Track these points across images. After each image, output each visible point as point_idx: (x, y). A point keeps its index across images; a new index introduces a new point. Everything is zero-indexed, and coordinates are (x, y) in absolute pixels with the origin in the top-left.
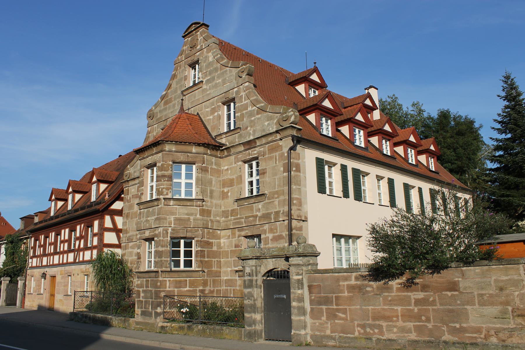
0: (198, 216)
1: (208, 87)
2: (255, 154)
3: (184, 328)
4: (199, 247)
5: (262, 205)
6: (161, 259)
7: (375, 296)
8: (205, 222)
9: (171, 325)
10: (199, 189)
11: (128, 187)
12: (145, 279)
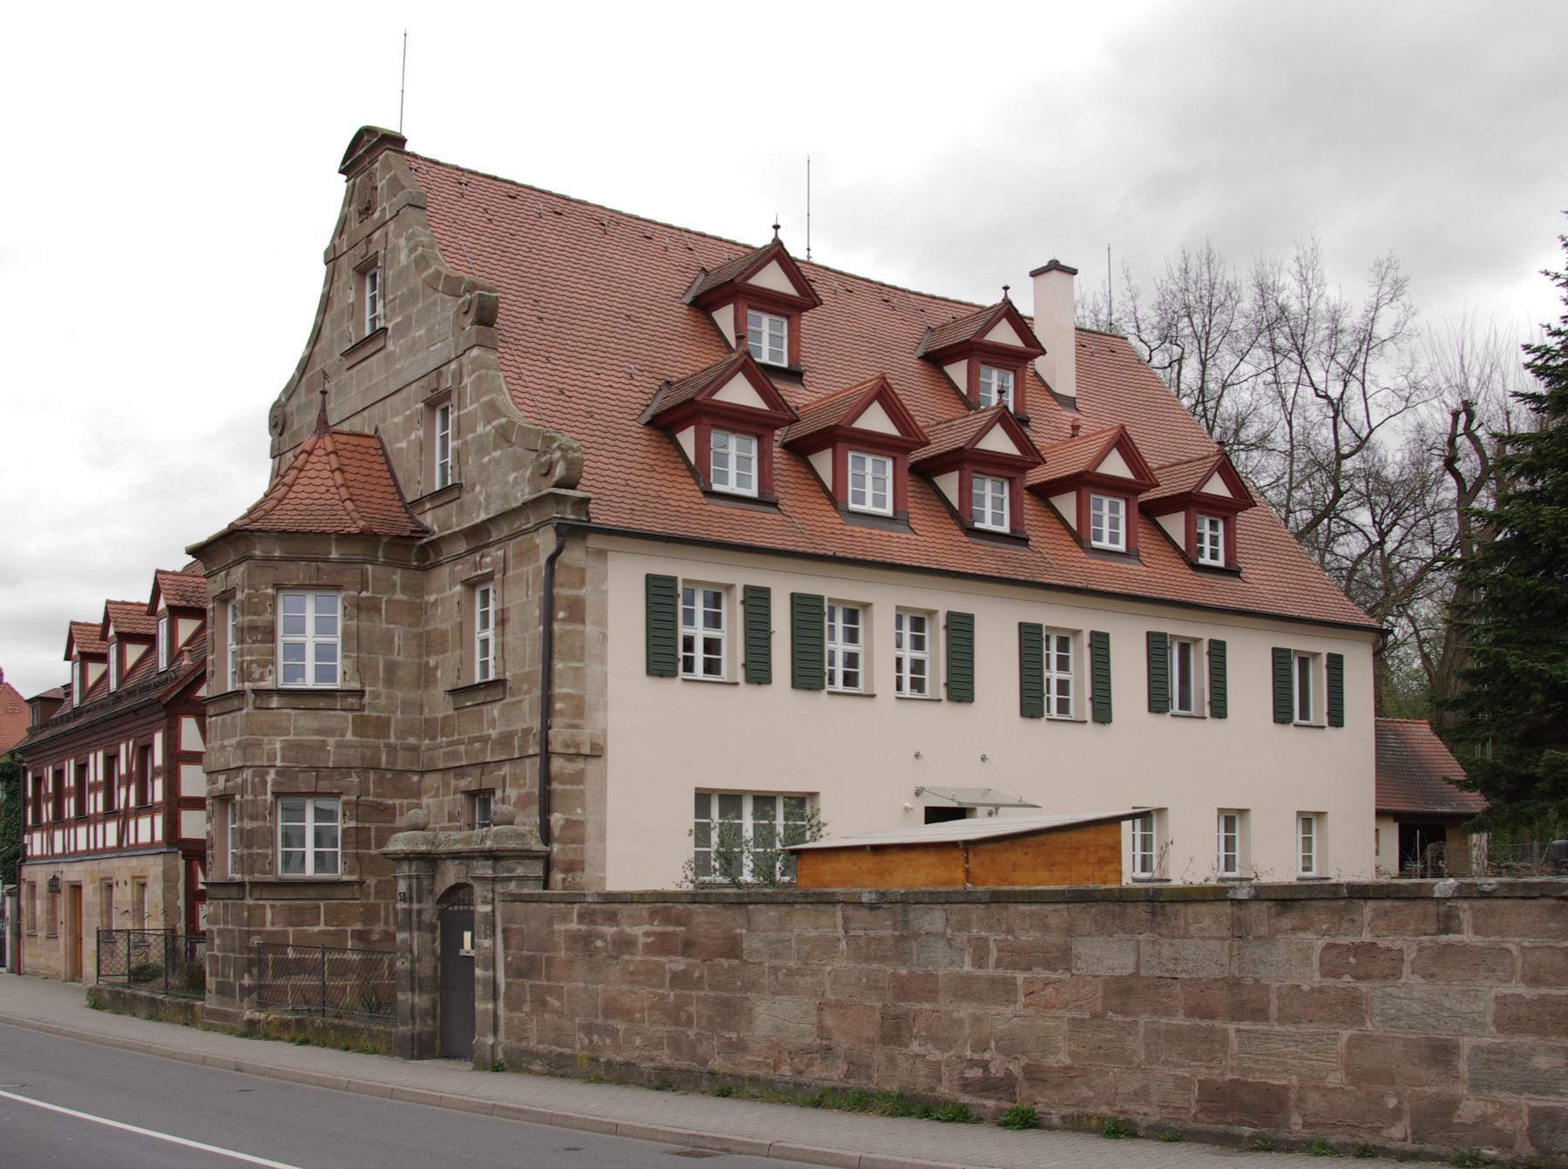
0: (349, 736)
1: (398, 350)
4: (351, 820)
6: (250, 851)
7: (609, 961)
8: (368, 753)
10: (349, 662)
12: (221, 902)
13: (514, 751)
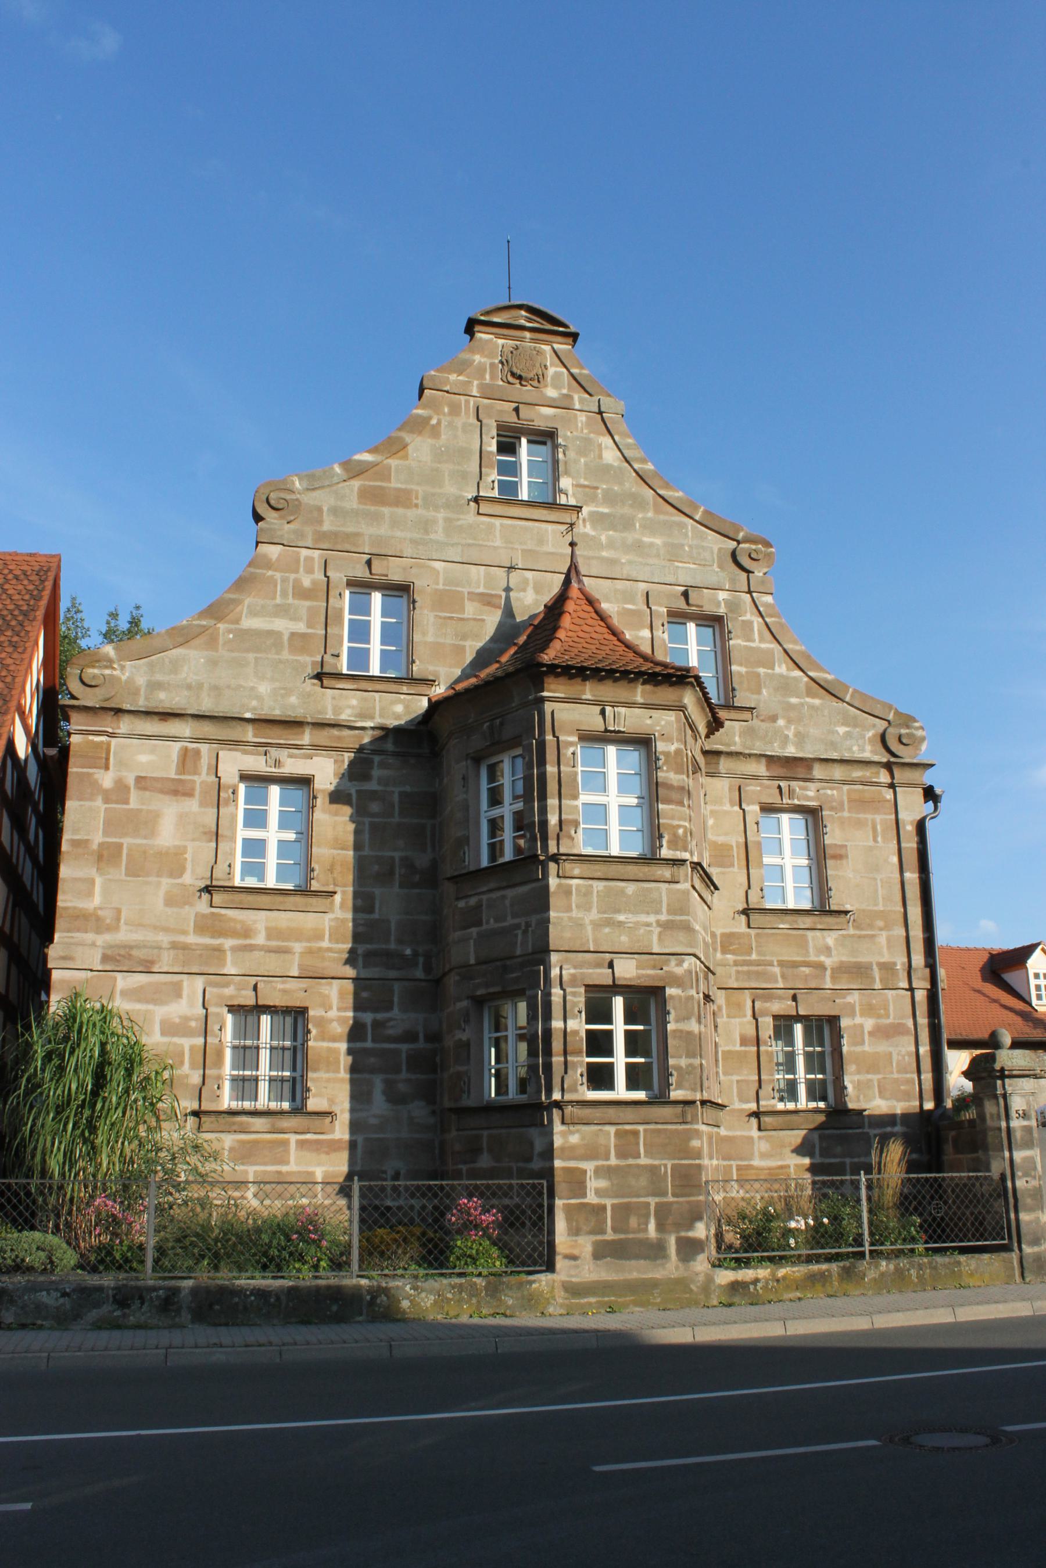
2: (808, 798)
5: (836, 939)
9: (773, 1274)
11: (112, 735)
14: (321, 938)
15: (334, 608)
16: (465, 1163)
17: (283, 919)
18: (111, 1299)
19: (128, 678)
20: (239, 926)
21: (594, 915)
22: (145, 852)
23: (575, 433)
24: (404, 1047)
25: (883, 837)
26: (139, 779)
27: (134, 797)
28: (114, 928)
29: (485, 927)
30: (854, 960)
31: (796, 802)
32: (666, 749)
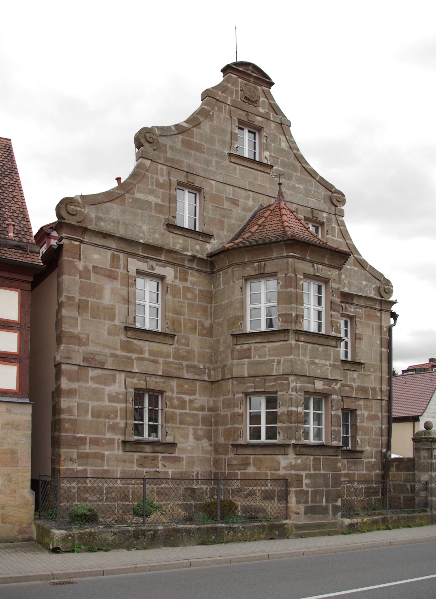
2: (351, 312)
3: (379, 522)
11: (81, 242)
13: (369, 395)
14: (169, 357)
15: (173, 195)
16: (240, 470)
17: (156, 347)
18: (133, 536)
19: (87, 213)
20: (138, 348)
21: (307, 359)
22: (98, 307)
23: (270, 131)
24: (200, 413)
25: (375, 333)
26: (94, 267)
27: (93, 277)
28: (86, 344)
29: (252, 359)
30: (362, 385)
31: (347, 313)
32: (335, 287)
